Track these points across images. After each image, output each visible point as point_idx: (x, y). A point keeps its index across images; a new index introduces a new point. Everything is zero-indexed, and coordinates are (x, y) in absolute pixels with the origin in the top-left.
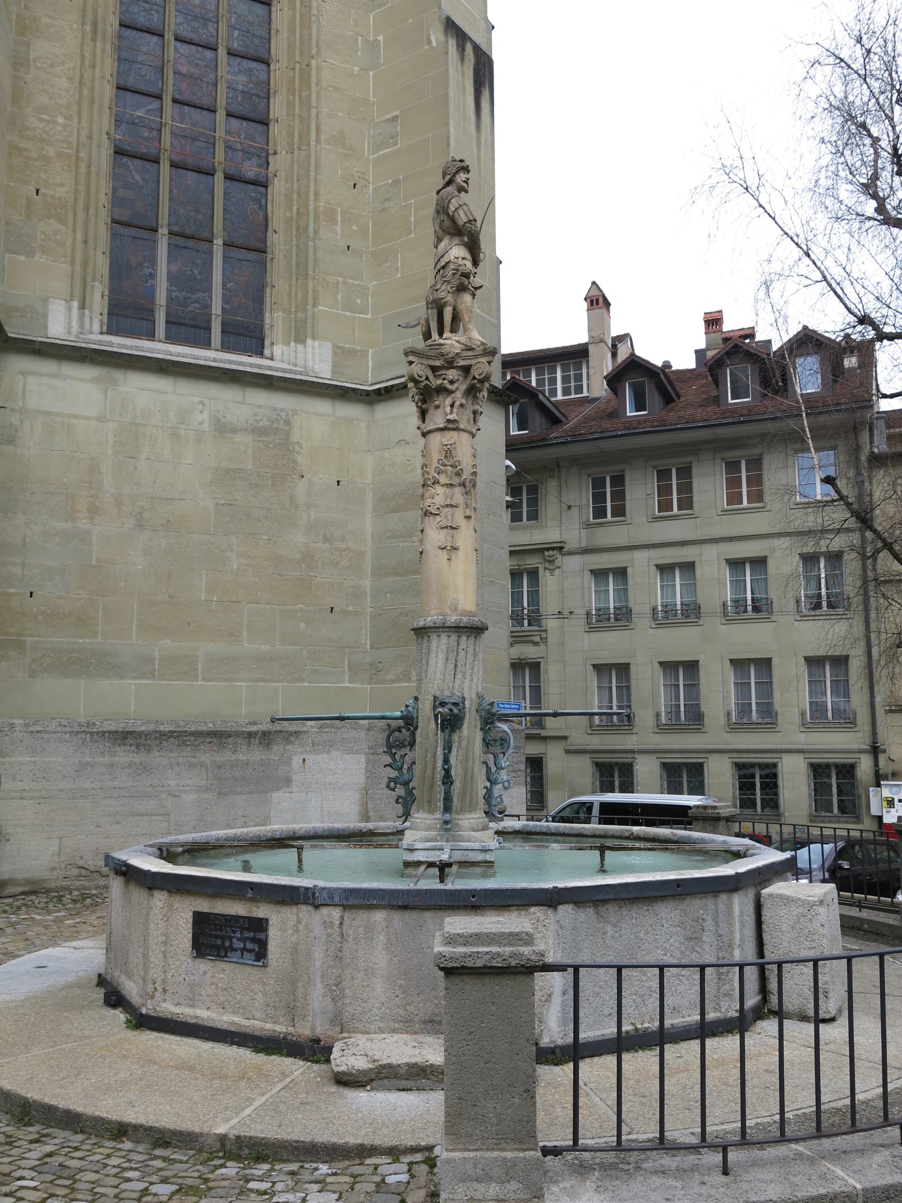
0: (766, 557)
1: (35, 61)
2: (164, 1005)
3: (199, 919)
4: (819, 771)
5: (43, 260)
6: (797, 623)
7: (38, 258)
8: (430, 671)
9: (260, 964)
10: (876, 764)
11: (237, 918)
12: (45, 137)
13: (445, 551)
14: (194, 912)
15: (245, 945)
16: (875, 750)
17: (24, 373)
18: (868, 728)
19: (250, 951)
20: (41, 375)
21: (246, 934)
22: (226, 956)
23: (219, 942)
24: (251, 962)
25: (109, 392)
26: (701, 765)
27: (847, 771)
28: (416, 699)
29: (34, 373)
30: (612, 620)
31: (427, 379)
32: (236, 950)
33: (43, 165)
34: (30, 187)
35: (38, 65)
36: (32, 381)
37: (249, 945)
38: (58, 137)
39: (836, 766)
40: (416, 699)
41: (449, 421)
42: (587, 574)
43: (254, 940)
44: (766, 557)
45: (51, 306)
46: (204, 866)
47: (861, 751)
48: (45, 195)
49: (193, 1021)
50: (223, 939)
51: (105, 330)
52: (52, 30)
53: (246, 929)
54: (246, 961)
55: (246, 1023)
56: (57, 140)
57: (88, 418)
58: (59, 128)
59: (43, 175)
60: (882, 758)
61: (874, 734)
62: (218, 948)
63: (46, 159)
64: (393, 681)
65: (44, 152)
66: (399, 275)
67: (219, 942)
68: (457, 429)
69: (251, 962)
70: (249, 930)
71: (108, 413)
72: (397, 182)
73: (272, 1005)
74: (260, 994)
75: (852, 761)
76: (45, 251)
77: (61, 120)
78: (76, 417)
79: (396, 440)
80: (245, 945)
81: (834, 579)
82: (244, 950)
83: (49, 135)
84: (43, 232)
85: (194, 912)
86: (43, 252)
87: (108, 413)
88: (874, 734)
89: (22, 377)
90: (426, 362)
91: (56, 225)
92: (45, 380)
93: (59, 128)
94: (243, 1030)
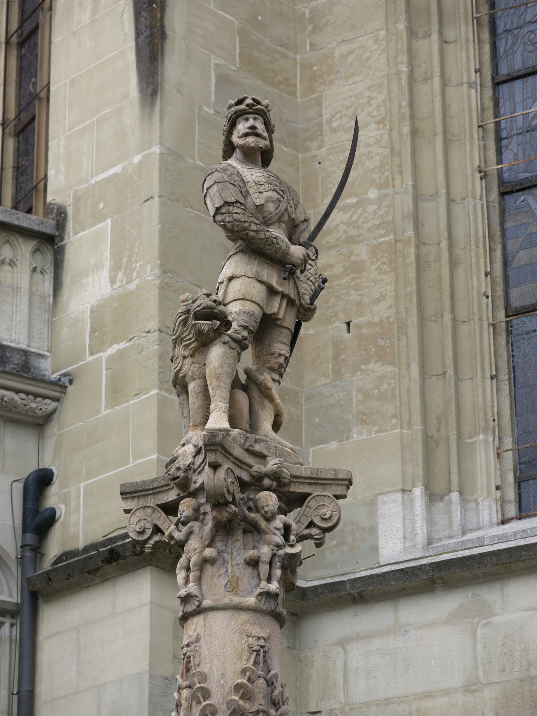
1: (329, 122)
5: (364, 437)
7: (358, 435)
12: (353, 232)
17: (342, 643)
20: (369, 637)
25: (479, 632)
29: (358, 638)
31: (157, 530)
33: (354, 279)
34: (337, 324)
35: (335, 125)
36: (356, 652)
38: (370, 224)
41: (185, 599)
45: (382, 510)
48: (359, 327)
51: (512, 510)
52: (351, 58)
56: (369, 230)
57: (448, 692)
58: (371, 208)
59: (354, 296)
63: (356, 268)
65: (354, 258)
68: (200, 611)
71: (481, 674)
76: (364, 419)
77: (373, 194)
78: (429, 695)
83: (358, 227)
84: (360, 390)
86: (363, 422)
87: (481, 674)
89: (340, 649)
90: (153, 501)
91: (377, 368)
92: (376, 644)
93: (371, 208)
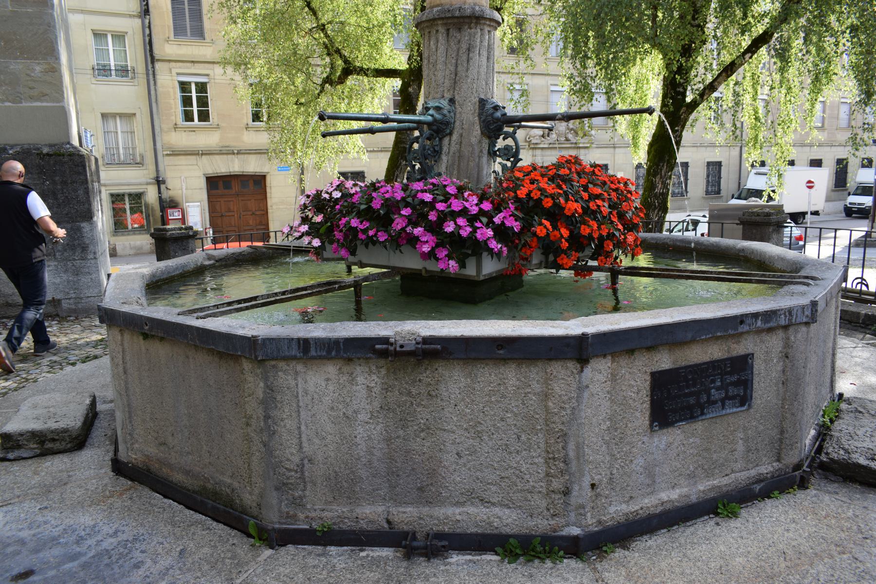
2: (612, 509)
8: (473, 72)
10: (160, 192)
11: (714, 365)
14: (653, 374)
16: (159, 182)
18: (152, 167)
19: (733, 398)
22: (702, 414)
23: (692, 401)
24: (735, 410)
28: (452, 101)
39: (130, 195)
40: (452, 101)
43: (736, 384)
49: (660, 509)
50: (697, 394)
54: (728, 411)
55: (725, 481)
60: (163, 187)
61: (157, 171)
67: (692, 401)
70: (731, 374)
74: (741, 442)
75: (141, 191)
85: (653, 374)
88: (157, 171)
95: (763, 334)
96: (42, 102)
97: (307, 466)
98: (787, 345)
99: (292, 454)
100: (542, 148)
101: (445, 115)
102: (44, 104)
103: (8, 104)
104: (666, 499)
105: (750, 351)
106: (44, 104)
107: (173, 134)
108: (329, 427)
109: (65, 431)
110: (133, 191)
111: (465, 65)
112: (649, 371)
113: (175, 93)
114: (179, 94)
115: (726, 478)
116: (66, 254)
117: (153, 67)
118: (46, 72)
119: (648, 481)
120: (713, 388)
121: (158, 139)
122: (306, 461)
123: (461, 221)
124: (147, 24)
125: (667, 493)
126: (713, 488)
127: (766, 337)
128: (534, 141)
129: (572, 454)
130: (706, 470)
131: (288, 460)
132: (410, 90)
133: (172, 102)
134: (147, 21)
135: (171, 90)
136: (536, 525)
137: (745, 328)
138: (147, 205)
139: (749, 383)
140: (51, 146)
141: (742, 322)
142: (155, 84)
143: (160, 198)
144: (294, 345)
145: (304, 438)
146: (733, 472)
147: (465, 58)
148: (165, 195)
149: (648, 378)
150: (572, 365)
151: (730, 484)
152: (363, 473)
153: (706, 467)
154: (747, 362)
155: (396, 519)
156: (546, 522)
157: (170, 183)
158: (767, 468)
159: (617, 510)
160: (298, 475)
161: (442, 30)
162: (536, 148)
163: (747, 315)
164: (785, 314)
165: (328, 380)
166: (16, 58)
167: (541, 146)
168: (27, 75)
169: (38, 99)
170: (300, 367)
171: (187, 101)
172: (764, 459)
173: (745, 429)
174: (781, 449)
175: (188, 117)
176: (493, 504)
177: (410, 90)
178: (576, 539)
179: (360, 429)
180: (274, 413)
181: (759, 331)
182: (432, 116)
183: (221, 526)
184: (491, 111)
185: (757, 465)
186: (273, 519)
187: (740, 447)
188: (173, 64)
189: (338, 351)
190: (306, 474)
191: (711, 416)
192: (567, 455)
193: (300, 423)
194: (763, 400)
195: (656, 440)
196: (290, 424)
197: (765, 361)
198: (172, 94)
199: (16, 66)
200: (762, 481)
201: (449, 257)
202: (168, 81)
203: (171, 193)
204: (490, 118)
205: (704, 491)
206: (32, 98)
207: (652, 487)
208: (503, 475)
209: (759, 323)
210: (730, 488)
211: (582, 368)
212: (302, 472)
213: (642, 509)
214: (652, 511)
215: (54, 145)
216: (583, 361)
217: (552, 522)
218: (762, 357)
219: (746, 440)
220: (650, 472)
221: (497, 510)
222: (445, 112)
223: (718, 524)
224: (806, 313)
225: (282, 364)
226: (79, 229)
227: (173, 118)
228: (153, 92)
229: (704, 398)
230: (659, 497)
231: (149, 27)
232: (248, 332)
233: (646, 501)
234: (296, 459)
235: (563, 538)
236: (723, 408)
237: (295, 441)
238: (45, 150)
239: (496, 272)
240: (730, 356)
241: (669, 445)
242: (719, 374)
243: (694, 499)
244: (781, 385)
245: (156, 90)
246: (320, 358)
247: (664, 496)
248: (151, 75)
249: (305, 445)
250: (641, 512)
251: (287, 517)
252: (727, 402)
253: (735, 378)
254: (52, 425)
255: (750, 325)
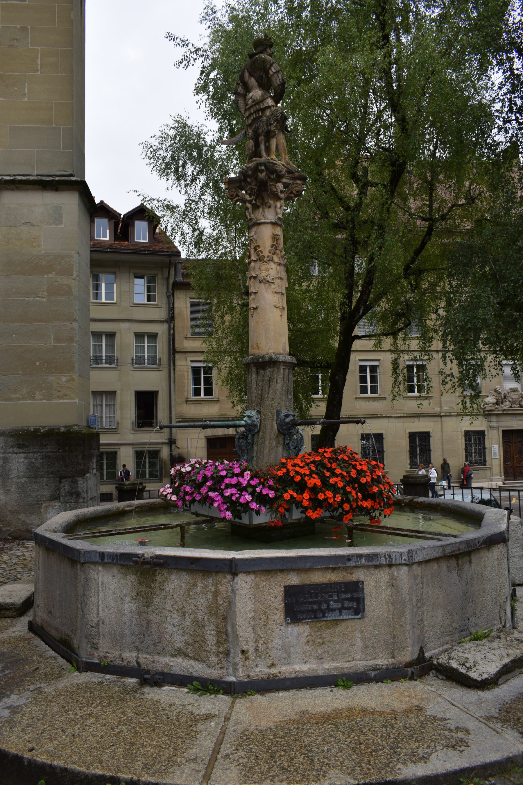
0: (115, 333)
2: (258, 669)
3: (290, 592)
4: (139, 455)
6: (131, 372)
9: (359, 617)
10: (171, 450)
11: (331, 587)
13: (278, 309)
14: (285, 587)
15: (343, 605)
16: (171, 442)
21: (343, 596)
22: (324, 616)
24: (350, 617)
26: (116, 453)
27: (155, 454)
30: (104, 363)
32: (333, 610)
37: (347, 604)
42: (133, 335)
43: (351, 600)
44: (115, 333)
46: (369, 544)
47: (163, 443)
49: (293, 676)
50: (320, 603)
53: (342, 592)
54: (345, 617)
55: (347, 665)
60: (174, 446)
62: (314, 612)
64: (19, 399)
66: (26, 99)
67: (315, 607)
69: (350, 617)
70: (345, 592)
72: (24, 29)
73: (371, 645)
74: (359, 640)
75: (158, 449)
79: (23, 221)
80: (343, 605)
81: (153, 349)
82: (343, 608)
85: (285, 587)
94: (346, 671)
95: (372, 569)
96: (64, 399)
97: (101, 625)
98: (393, 578)
99: (94, 617)
100: (497, 415)
101: (254, 421)
102: (65, 401)
103: (44, 401)
104: (298, 669)
105: (361, 579)
106: (65, 401)
107: (185, 405)
108: (112, 603)
109: (13, 604)
110: (152, 449)
111: (267, 390)
112: (283, 585)
113: (188, 375)
114: (191, 376)
115: (348, 663)
116: (66, 498)
117: (174, 357)
118: (68, 381)
119: (284, 655)
120: (332, 600)
121: (173, 409)
122: (101, 622)
123: (234, 491)
124: (172, 327)
125: (300, 666)
126: (336, 668)
127: (375, 572)
128: (488, 408)
129: (229, 629)
130: (331, 655)
131: (92, 620)
132: (337, 377)
133: (186, 382)
134: (172, 325)
135: (186, 373)
136: (211, 673)
137: (352, 564)
138: (161, 461)
139: (361, 600)
140: (65, 427)
141: (349, 560)
142: (174, 369)
143: (171, 454)
144: (98, 554)
145: (100, 609)
146: (353, 659)
147: (267, 386)
148: (175, 452)
149: (283, 589)
150: (229, 577)
151: (350, 668)
152: (127, 632)
153: (331, 653)
154: (358, 586)
155: (141, 661)
156: (216, 671)
157: (179, 443)
158: (383, 661)
159: (260, 670)
160: (96, 630)
161: (254, 369)
162: (490, 415)
163: (352, 556)
164: (385, 556)
165: (114, 576)
166: (52, 373)
167: (496, 412)
168: (58, 383)
169: (62, 398)
170: (100, 568)
171: (197, 381)
172: (381, 655)
173: (362, 632)
174: (394, 650)
175: (197, 392)
176: (191, 658)
177: (337, 377)
178: (230, 683)
179: (127, 606)
180: (87, 593)
181: (368, 567)
182: (245, 421)
183: (64, 660)
184: (283, 418)
185: (375, 658)
186: (84, 657)
187: (359, 643)
188: (189, 354)
189: (117, 560)
190: (101, 630)
191: (331, 619)
192: (227, 630)
193: (98, 599)
194: (376, 614)
195: (290, 629)
196: (94, 599)
197: (375, 587)
198: (186, 376)
199: (52, 378)
200: (377, 670)
201: (227, 509)
202: (184, 365)
203: (179, 450)
204: (282, 422)
205: (328, 669)
206: (59, 397)
207: (288, 659)
208: (195, 639)
209: (363, 561)
210: (351, 671)
211: (234, 578)
212: (98, 629)
213: (280, 673)
214: (288, 675)
215: (69, 426)
216: (235, 574)
217: (220, 672)
218: (372, 584)
219: (363, 639)
220: (286, 648)
221: (192, 662)
222: (254, 419)
223: (331, 691)
224: (404, 558)
225: (92, 566)
226: (76, 482)
227: (186, 393)
228: (172, 375)
229: (324, 606)
230: (293, 667)
231: (174, 329)
232: (78, 547)
233: (283, 668)
234: (95, 620)
235: (224, 682)
236: (341, 614)
237: (95, 610)
238: (62, 430)
239: (265, 523)
240: (345, 580)
241: (299, 634)
242: (335, 592)
243: (321, 673)
244: (390, 605)
245: (174, 373)
246: (109, 563)
247: (297, 667)
248: (172, 362)
249: (101, 612)
250: (279, 675)
251: (90, 655)
252: (343, 611)
253: (349, 596)
254: (8, 600)
255: (356, 562)
